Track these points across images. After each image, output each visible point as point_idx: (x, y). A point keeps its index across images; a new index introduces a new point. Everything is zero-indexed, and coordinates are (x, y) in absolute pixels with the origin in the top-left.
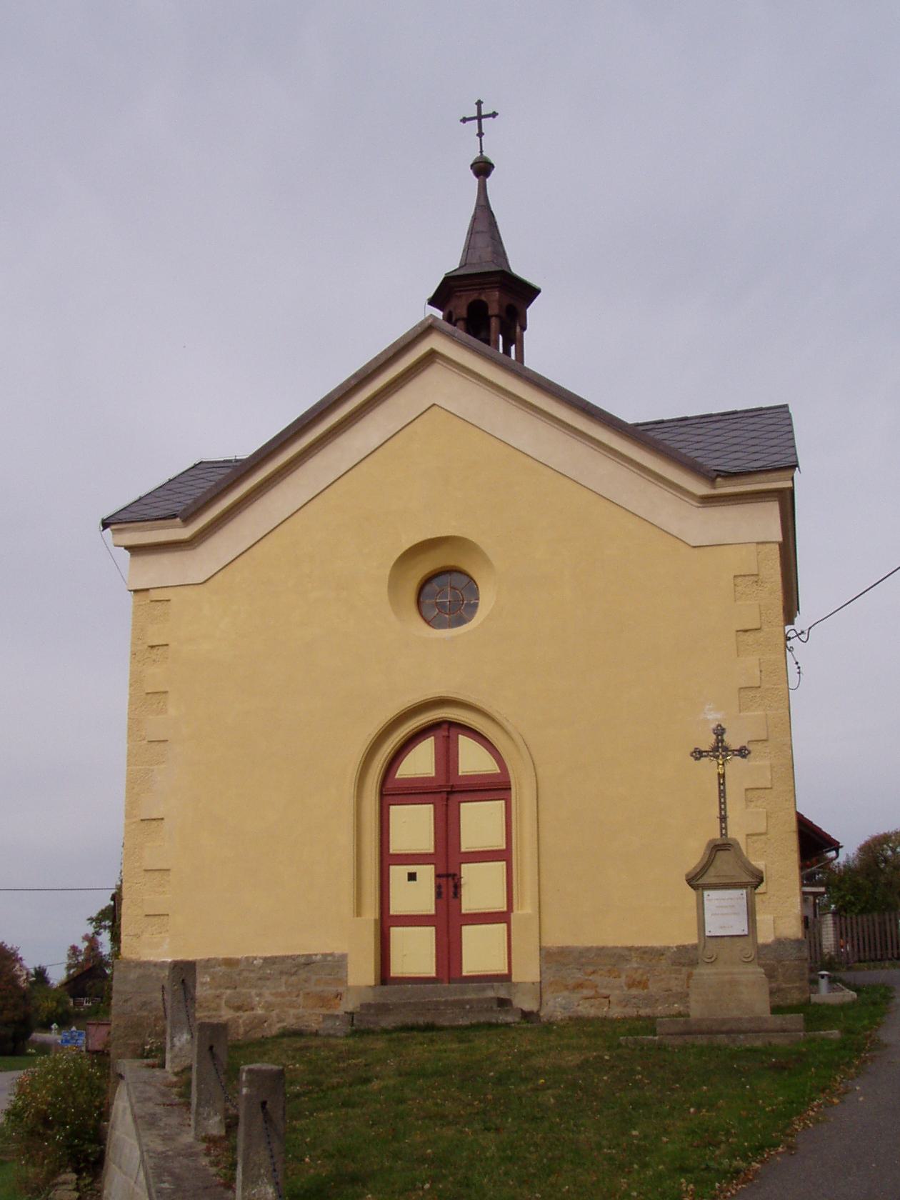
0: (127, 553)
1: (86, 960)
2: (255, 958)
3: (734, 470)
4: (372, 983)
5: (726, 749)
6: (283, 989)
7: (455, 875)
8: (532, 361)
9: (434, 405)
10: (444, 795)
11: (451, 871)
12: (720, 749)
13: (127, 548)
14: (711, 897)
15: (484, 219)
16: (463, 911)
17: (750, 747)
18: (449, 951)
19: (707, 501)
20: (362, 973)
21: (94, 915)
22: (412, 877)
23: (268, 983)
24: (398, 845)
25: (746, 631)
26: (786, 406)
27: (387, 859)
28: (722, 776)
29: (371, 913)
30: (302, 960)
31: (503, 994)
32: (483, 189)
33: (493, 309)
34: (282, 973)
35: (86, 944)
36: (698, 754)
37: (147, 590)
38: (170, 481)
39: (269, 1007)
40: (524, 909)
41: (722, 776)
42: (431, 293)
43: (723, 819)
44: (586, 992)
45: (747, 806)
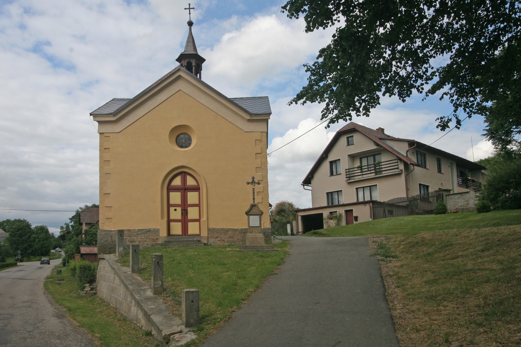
0: (97, 123)
1: (66, 230)
2: (136, 229)
3: (256, 113)
4: (166, 236)
5: (255, 182)
6: (143, 237)
7: (186, 210)
8: (203, 79)
9: (180, 90)
10: (183, 190)
11: (185, 209)
12: (253, 182)
13: (97, 121)
14: (251, 217)
15: (191, 39)
16: (188, 219)
17: (260, 182)
18: (185, 229)
19: (249, 121)
20: (163, 233)
21: (71, 217)
22: (175, 210)
23: (139, 235)
24: (172, 202)
25: (258, 154)
26: (268, 97)
27: (169, 205)
28: (254, 189)
29: (166, 219)
30: (148, 230)
31: (199, 239)
32: (190, 30)
33: (194, 64)
34: (143, 233)
35: (66, 226)
36: (248, 183)
37: (103, 133)
38: (107, 103)
39: (139, 242)
40: (204, 219)
41: (254, 189)
42: (177, 57)
43: (254, 199)
44: (219, 239)
45: (257, 196)
